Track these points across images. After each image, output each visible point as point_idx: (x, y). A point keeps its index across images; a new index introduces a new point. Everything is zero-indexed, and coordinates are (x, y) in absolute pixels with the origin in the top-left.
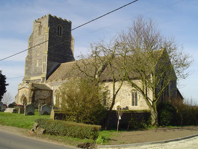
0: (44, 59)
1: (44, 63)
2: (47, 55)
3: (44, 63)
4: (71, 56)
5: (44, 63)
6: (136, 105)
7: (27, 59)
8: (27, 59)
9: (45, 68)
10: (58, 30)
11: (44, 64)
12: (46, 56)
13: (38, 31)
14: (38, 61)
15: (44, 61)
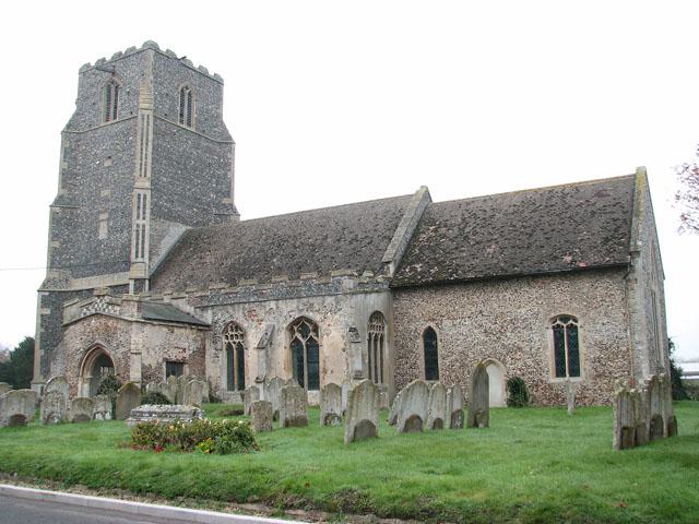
0: (139, 207)
1: (138, 222)
2: (149, 193)
3: (141, 222)
4: (225, 201)
5: (138, 222)
6: (575, 372)
7: (57, 210)
8: (57, 210)
9: (143, 241)
10: (182, 105)
11: (138, 226)
12: (145, 196)
13: (102, 105)
14: (103, 216)
15: (138, 217)
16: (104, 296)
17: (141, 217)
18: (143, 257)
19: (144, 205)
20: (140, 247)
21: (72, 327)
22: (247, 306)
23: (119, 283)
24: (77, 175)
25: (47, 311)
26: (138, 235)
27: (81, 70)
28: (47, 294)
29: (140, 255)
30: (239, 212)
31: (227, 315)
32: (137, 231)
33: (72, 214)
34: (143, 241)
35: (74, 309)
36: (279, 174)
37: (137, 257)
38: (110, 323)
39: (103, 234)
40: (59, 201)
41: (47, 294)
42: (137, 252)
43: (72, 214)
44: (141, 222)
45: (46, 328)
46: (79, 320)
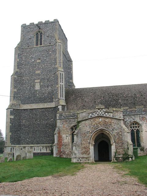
0: (61, 78)
1: (61, 83)
5: (61, 83)
8: (16, 77)
16: (102, 109)
17: (62, 82)
18: (63, 97)
19: (62, 78)
20: (62, 91)
21: (83, 122)
22: (141, 115)
23: (47, 107)
24: (23, 64)
25: (12, 117)
26: (61, 89)
27: (22, 26)
28: (12, 110)
29: (62, 96)
30: (75, 85)
31: (131, 119)
32: (61, 87)
33: (21, 79)
34: (63, 91)
35: (84, 114)
36: (89, 73)
37: (61, 97)
38: (107, 120)
39: (37, 87)
40: (16, 73)
41: (12, 110)
42: (61, 95)
43: (21, 79)
44: (62, 84)
45: (12, 124)
46: (88, 119)
